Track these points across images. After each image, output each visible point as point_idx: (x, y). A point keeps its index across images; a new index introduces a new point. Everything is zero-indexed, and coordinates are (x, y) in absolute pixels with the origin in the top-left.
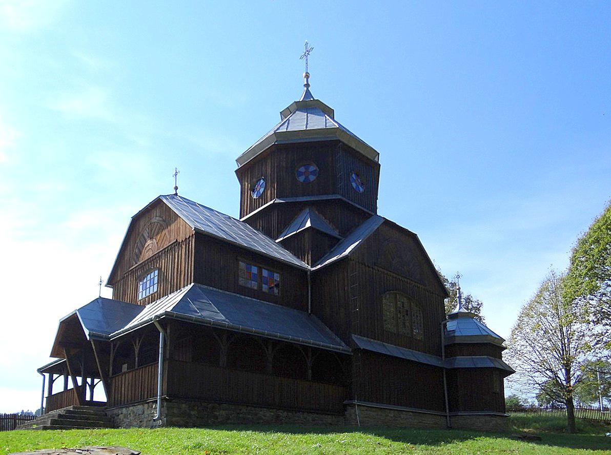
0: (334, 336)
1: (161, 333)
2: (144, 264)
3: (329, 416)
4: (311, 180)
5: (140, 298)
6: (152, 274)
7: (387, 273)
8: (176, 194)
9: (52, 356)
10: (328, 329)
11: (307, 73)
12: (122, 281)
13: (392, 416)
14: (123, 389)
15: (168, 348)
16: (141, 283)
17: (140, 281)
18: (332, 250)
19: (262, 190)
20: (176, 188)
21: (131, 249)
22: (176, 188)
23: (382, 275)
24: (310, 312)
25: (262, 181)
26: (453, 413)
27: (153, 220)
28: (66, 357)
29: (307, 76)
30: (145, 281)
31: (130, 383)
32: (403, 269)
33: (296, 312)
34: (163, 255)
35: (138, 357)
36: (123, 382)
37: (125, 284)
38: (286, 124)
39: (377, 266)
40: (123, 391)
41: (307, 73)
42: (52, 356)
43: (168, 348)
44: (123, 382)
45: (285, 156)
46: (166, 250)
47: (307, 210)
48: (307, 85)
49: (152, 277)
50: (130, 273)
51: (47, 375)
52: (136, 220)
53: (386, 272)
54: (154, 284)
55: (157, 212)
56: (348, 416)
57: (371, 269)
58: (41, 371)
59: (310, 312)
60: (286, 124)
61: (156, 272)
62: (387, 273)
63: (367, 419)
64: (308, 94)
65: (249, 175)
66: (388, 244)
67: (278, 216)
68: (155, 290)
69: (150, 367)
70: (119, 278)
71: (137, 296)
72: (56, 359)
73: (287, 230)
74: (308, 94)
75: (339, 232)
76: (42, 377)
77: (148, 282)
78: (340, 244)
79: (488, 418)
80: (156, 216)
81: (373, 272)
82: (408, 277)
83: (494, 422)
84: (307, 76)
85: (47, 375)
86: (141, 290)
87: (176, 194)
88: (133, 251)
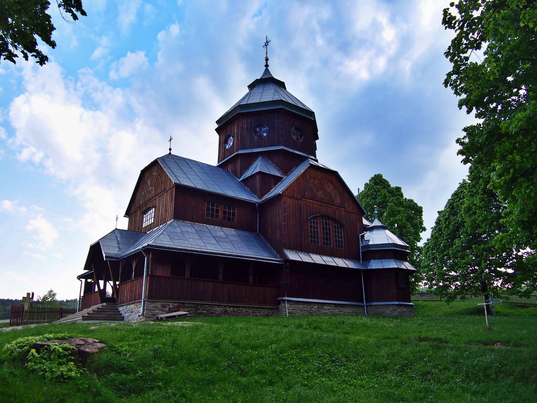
0: (273, 250)
1: (146, 258)
2: (147, 203)
3: (266, 310)
4: (265, 136)
5: (144, 226)
6: (151, 210)
7: (313, 202)
8: (170, 153)
9: (85, 269)
10: (269, 245)
11: (267, 57)
12: (134, 214)
13: (317, 307)
14: (125, 293)
15: (150, 267)
16: (145, 216)
17: (144, 214)
18: (276, 186)
19: (231, 144)
20: (170, 149)
21: (140, 192)
22: (170, 149)
23: (309, 204)
24: (258, 233)
25: (231, 138)
26: (369, 304)
27: (154, 174)
28: (93, 269)
29: (267, 60)
30: (147, 215)
31: (129, 289)
32: (326, 198)
33: (246, 233)
34: (158, 198)
35: (134, 272)
36: (126, 288)
37: (136, 216)
38: (249, 96)
39: (304, 198)
40: (125, 295)
41: (267, 57)
42: (85, 269)
43: (150, 267)
44: (126, 288)
45: (246, 120)
46: (160, 195)
47: (260, 158)
48: (267, 66)
49: (151, 212)
50: (139, 208)
51: (83, 280)
52: (144, 172)
53: (311, 201)
54: (152, 218)
55: (155, 169)
56: (280, 308)
57: (300, 201)
58: (79, 277)
59: (258, 233)
60: (249, 96)
61: (154, 209)
62: (313, 202)
63: (295, 311)
64: (267, 71)
65: (224, 133)
66: (314, 181)
67: (241, 163)
68: (152, 222)
69: (122, 285)
70: (132, 212)
71: (142, 225)
72: (87, 271)
73: (246, 172)
74: (267, 71)
75: (282, 172)
76: (80, 282)
77: (149, 216)
78: (283, 181)
79: (395, 307)
80: (155, 171)
81: (301, 203)
82: (330, 203)
83: (399, 310)
84: (267, 60)
85: (83, 280)
86: (144, 221)
87: (170, 153)
88: (141, 193)
